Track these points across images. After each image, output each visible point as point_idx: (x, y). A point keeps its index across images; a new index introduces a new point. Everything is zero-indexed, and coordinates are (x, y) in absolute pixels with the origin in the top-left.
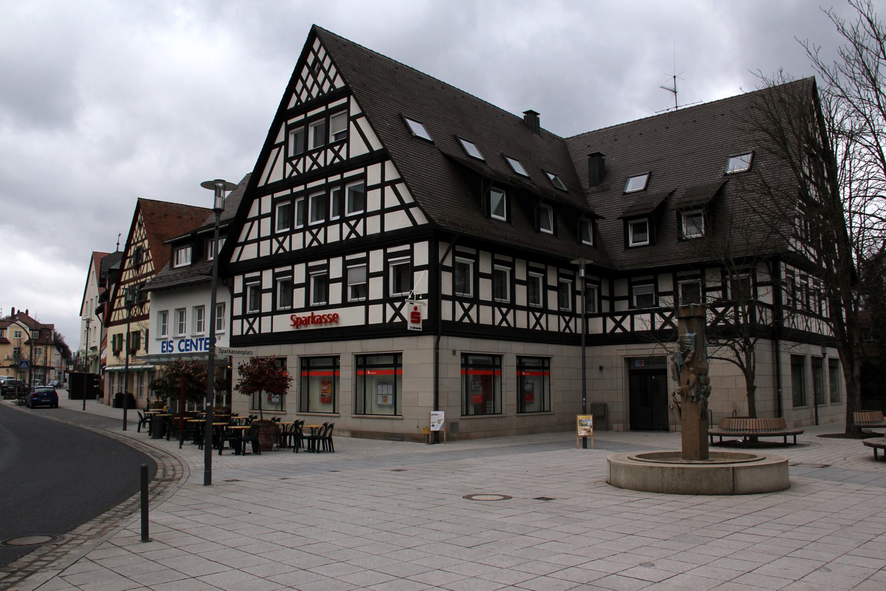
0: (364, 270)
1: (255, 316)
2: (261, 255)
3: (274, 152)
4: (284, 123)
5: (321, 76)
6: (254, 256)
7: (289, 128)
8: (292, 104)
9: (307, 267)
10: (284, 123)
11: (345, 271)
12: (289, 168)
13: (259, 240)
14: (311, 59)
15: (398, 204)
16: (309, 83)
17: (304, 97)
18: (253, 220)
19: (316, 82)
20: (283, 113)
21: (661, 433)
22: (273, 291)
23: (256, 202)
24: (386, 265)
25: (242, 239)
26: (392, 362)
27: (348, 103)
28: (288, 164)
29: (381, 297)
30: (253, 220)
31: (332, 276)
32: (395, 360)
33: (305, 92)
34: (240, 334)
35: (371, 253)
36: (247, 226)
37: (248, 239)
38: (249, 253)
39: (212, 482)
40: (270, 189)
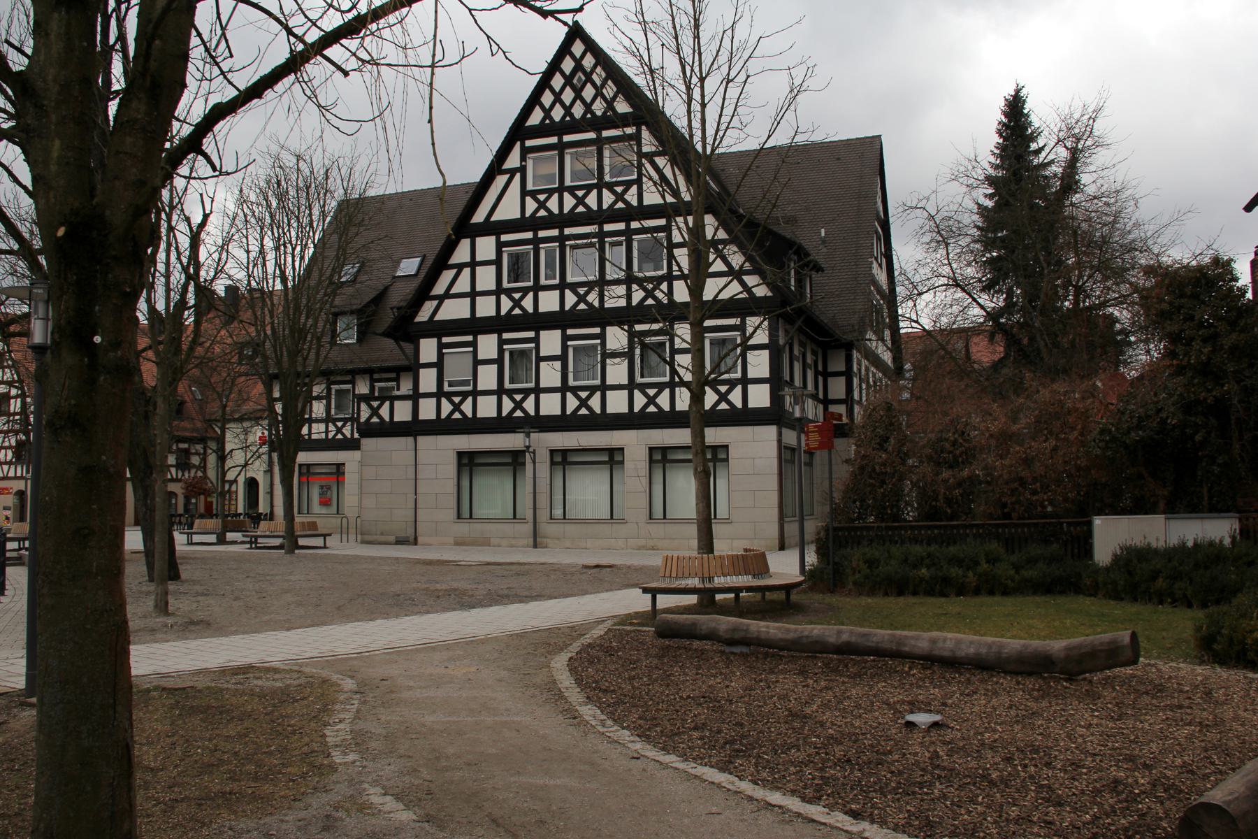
0: (471, 356)
2: (753, 289)
3: (501, 180)
5: (588, 92)
7: (525, 152)
8: (536, 118)
9: (439, 343)
11: (441, 356)
12: (531, 205)
14: (568, 65)
16: (568, 96)
18: (460, 267)
19: (578, 96)
20: (519, 131)
22: (499, 361)
23: (465, 244)
26: (335, 471)
27: (639, 132)
29: (434, 390)
32: (338, 469)
35: (542, 333)
37: (451, 292)
38: (455, 310)
40: (492, 228)
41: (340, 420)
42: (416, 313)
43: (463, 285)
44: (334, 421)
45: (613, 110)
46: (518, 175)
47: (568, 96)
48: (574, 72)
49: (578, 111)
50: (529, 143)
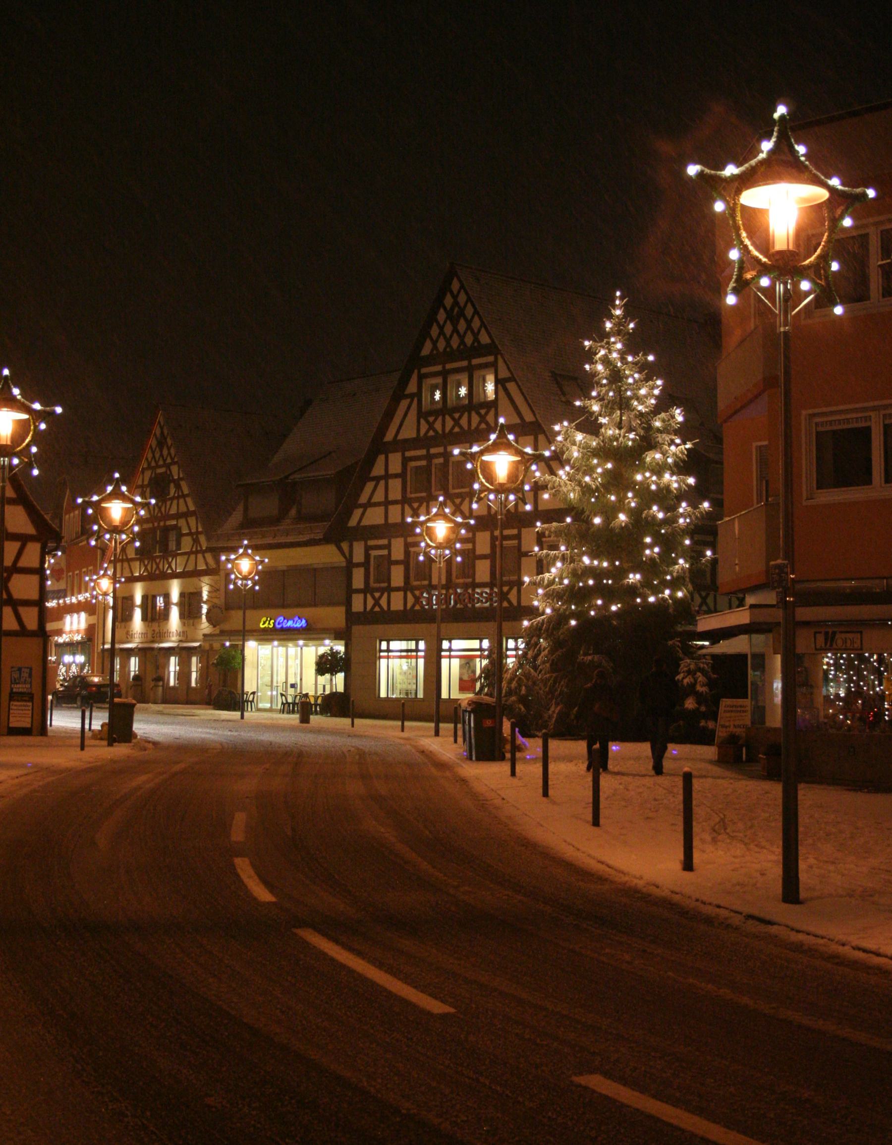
1: (382, 591)
3: (404, 403)
4: (416, 371)
5: (462, 326)
6: (380, 521)
10: (416, 371)
12: (424, 427)
13: (387, 503)
15: (373, 501)
16: (448, 329)
17: (441, 345)
18: (377, 479)
19: (455, 330)
21: (63, 712)
23: (381, 459)
24: (367, 556)
25: (363, 499)
28: (422, 421)
29: (362, 586)
30: (377, 479)
31: (394, 557)
33: (448, 334)
34: (402, 608)
36: (370, 486)
39: (664, 771)
41: (378, 590)
42: (384, 435)
43: (379, 497)
44: (412, 589)
45: (479, 342)
46: (416, 400)
47: (448, 329)
48: (452, 308)
49: (455, 343)
50: (424, 370)
